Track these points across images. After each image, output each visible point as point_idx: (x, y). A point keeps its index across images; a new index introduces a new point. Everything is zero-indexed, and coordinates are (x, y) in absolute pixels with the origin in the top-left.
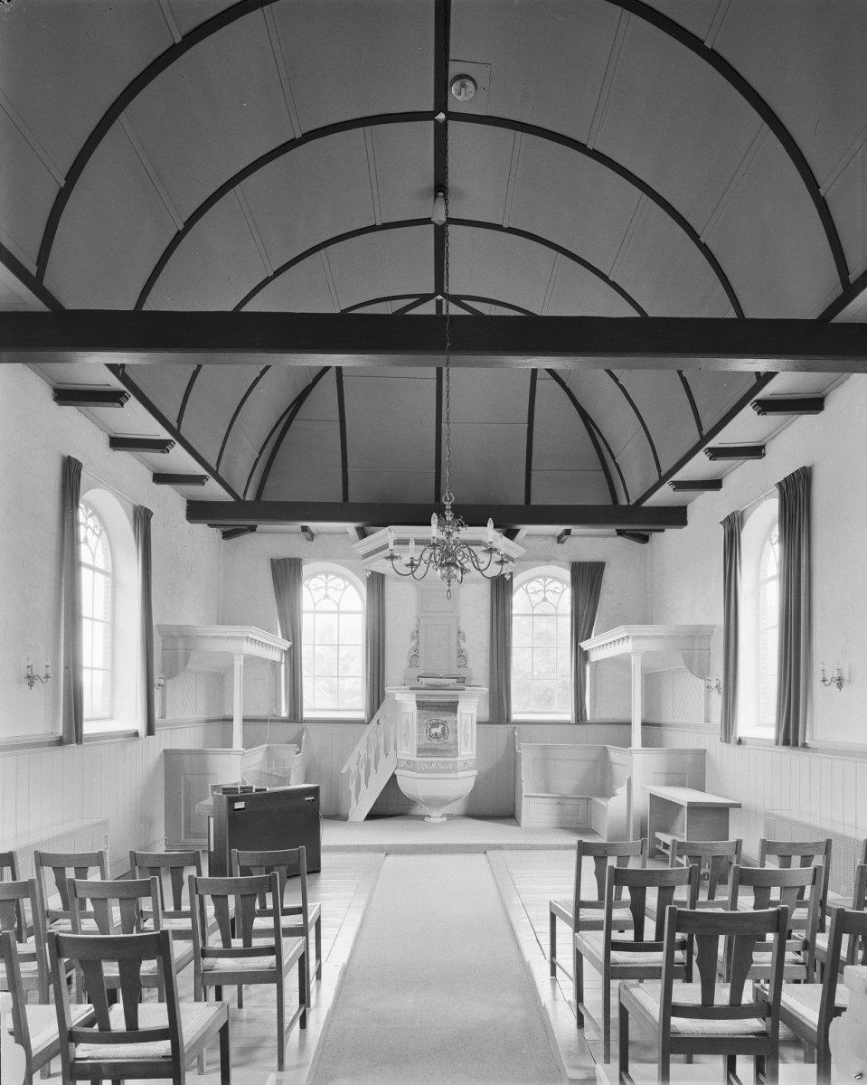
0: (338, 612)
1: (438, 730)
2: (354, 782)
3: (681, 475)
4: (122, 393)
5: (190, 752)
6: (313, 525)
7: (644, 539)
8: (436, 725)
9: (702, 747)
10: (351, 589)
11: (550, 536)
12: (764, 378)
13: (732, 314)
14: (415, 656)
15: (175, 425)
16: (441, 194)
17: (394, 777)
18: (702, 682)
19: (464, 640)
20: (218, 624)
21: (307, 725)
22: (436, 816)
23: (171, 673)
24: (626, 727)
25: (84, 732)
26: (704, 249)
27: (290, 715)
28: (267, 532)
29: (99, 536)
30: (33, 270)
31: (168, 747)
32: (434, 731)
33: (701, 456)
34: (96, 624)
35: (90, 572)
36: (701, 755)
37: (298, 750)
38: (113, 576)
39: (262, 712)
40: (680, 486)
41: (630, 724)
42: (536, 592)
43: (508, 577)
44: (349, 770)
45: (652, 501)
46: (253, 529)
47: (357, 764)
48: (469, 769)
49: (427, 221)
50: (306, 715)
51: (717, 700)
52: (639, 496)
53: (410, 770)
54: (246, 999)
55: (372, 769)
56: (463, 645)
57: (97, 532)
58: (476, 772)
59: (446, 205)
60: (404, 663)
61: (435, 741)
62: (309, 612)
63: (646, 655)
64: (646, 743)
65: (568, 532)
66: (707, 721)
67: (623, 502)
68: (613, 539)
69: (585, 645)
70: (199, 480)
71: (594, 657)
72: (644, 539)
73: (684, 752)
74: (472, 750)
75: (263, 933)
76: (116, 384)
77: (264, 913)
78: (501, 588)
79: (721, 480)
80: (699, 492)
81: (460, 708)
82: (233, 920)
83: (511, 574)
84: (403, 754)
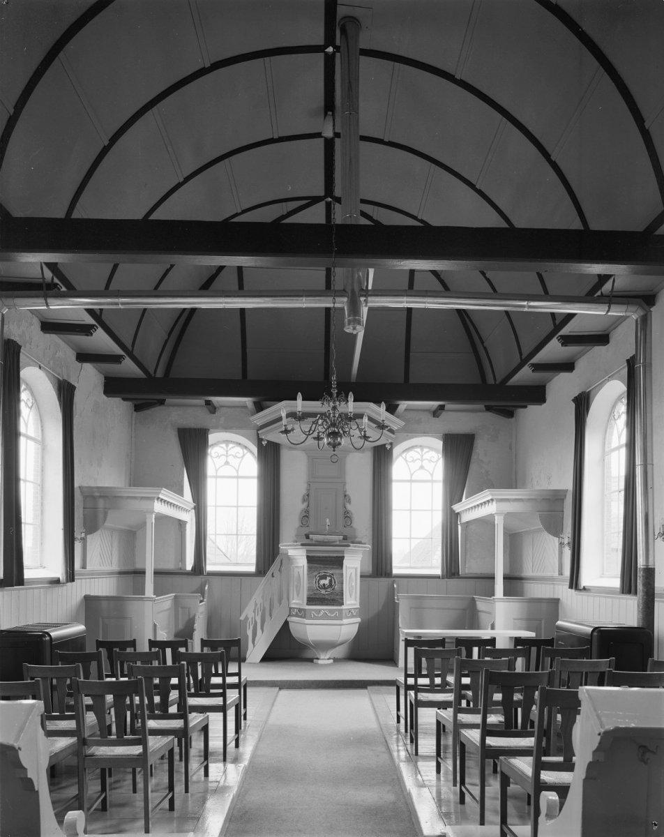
0: (238, 477)
1: (326, 582)
2: (251, 627)
3: (540, 357)
4: (94, 325)
5: (107, 598)
6: (216, 400)
7: (509, 414)
8: (324, 577)
9: (556, 597)
10: (249, 456)
11: (427, 410)
12: (603, 279)
13: (576, 225)
14: (305, 516)
15: (130, 348)
16: (330, 113)
17: (286, 623)
18: (556, 539)
19: (350, 502)
20: (130, 486)
21: (211, 578)
22: (324, 658)
23: (92, 527)
24: (488, 582)
25: (25, 577)
26: (554, 166)
27: (194, 568)
28: (174, 405)
29: (31, 408)
31: (88, 593)
32: (322, 582)
33: (554, 344)
34: (28, 483)
35: (25, 439)
36: (555, 602)
37: (202, 599)
38: (43, 444)
39: (170, 565)
40: (538, 367)
41: (494, 578)
42: (413, 461)
43: (388, 447)
44: (247, 618)
45: (517, 379)
46: (162, 402)
47: (254, 612)
48: (353, 616)
49: (318, 135)
50: (209, 568)
51: (568, 553)
52: (503, 377)
53: (301, 617)
54: (176, 772)
55: (259, 631)
56: (349, 507)
57: (30, 405)
58: (359, 620)
59: (334, 120)
60: (297, 524)
61: (323, 592)
62: (211, 477)
63: (508, 516)
64: (507, 593)
65: (442, 408)
66: (561, 573)
67: (490, 381)
68: (481, 414)
69: (457, 508)
70: (116, 359)
71: (466, 518)
72: (509, 414)
73: (540, 600)
74: (356, 600)
75: (216, 686)
76: (89, 320)
77: (217, 675)
78: (382, 456)
79: (574, 363)
80: (588, 348)
81: (345, 562)
82: (201, 680)
83: (391, 444)
84: (295, 603)
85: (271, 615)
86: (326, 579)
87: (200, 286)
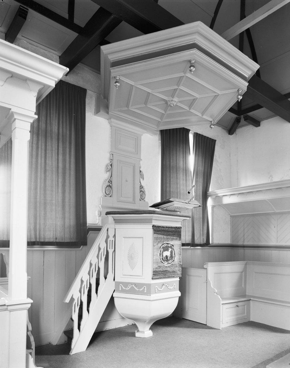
1: (167, 253)
8: (166, 249)
30: (66, 16)
44: (72, 299)
47: (80, 292)
61: (166, 264)
85: (88, 311)
86: (168, 250)
87: (107, 114)
